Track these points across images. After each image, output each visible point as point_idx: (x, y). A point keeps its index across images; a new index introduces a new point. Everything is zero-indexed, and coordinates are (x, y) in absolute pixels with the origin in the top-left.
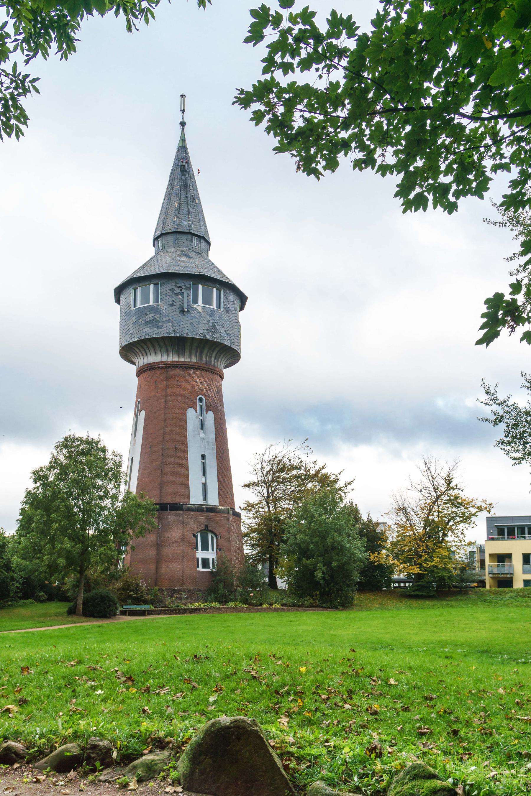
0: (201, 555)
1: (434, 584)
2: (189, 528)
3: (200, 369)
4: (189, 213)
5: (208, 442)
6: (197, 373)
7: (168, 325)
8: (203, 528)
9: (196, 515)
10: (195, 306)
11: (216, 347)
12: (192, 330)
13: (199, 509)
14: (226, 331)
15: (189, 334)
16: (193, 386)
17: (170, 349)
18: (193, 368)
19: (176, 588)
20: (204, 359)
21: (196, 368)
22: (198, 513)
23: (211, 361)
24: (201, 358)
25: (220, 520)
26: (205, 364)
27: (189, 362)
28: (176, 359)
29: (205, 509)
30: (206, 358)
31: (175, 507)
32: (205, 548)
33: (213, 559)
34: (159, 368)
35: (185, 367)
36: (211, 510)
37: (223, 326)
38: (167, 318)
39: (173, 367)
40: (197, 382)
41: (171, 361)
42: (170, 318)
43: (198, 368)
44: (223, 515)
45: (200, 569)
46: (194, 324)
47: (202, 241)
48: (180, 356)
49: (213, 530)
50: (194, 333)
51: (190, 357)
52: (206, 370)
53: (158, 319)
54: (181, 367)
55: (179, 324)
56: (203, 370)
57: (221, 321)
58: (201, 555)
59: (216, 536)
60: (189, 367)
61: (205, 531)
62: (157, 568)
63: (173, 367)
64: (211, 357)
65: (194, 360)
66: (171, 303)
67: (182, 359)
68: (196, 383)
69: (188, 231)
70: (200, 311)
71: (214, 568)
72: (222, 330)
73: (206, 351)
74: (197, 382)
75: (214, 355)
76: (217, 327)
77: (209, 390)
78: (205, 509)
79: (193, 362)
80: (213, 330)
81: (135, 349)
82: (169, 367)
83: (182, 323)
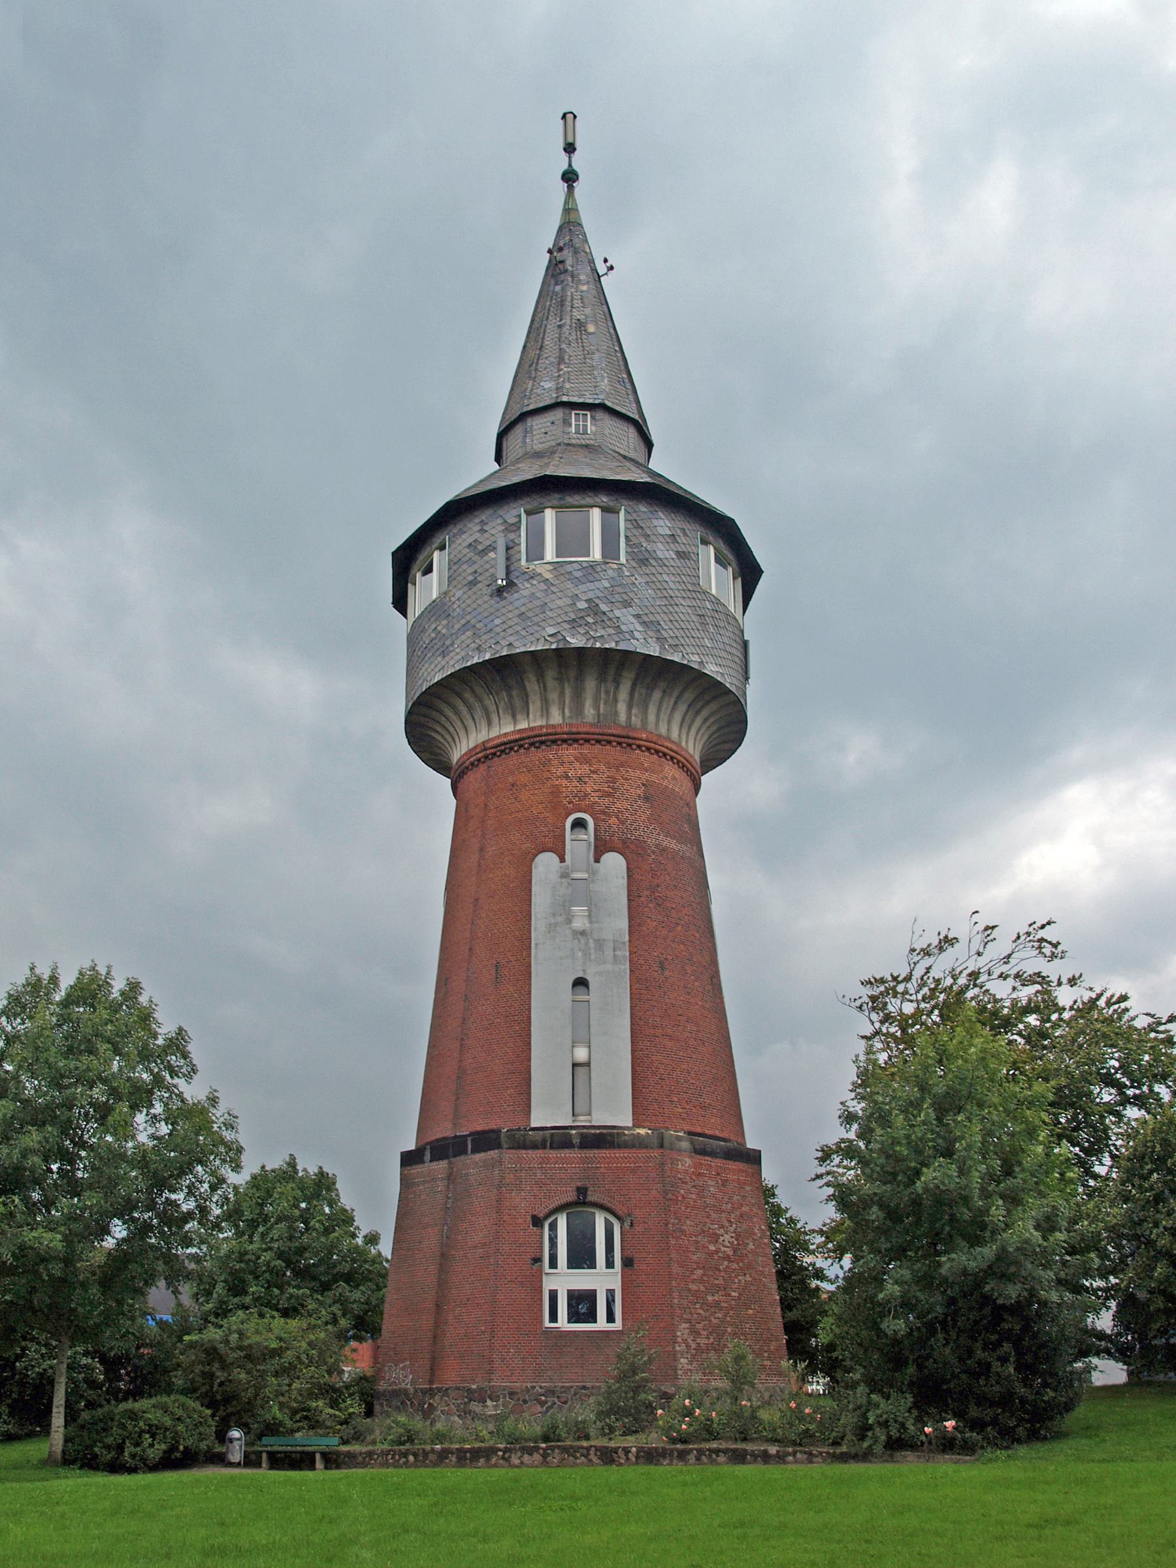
0: (563, 1280)
1: (634, 1449)
2: (522, 1203)
3: (576, 741)
4: (561, 360)
5: (600, 944)
6: (569, 752)
7: (463, 637)
8: (571, 1196)
9: (546, 1160)
10: (537, 566)
11: (715, 698)
12: (523, 633)
13: (558, 1139)
14: (638, 616)
15: (516, 644)
16: (556, 792)
17: (490, 703)
18: (554, 742)
19: (474, 1387)
20: (589, 712)
21: (565, 741)
22: (553, 1154)
23: (616, 714)
24: (578, 710)
25: (633, 1171)
26: (591, 725)
27: (541, 727)
28: (508, 728)
29: (576, 1141)
30: (596, 707)
31: (486, 1141)
32: (582, 1257)
33: (610, 1294)
34: (472, 764)
35: (531, 744)
36: (601, 1139)
37: (627, 604)
38: (463, 622)
39: (502, 751)
40: (567, 777)
41: (498, 737)
42: (468, 618)
43: (572, 739)
44: (642, 1154)
45: (547, 1324)
46: (530, 614)
47: (600, 415)
48: (519, 717)
49: (606, 1201)
50: (531, 638)
51: (545, 711)
52: (599, 741)
53: (444, 631)
54: (521, 746)
55: (490, 627)
56: (588, 741)
57: (619, 589)
58: (563, 1280)
59: (619, 1218)
60: (542, 743)
61: (580, 1203)
62: (437, 1324)
63: (502, 751)
64: (616, 700)
65: (556, 718)
66: (471, 578)
67: (523, 725)
68: (564, 782)
69: (553, 401)
70: (548, 576)
71: (611, 1318)
72: (626, 618)
73: (590, 684)
74: (567, 777)
75: (623, 695)
76: (604, 607)
77: (609, 795)
78: (576, 1141)
79: (553, 726)
80: (590, 620)
81: (433, 734)
82: (494, 754)
83: (497, 622)
